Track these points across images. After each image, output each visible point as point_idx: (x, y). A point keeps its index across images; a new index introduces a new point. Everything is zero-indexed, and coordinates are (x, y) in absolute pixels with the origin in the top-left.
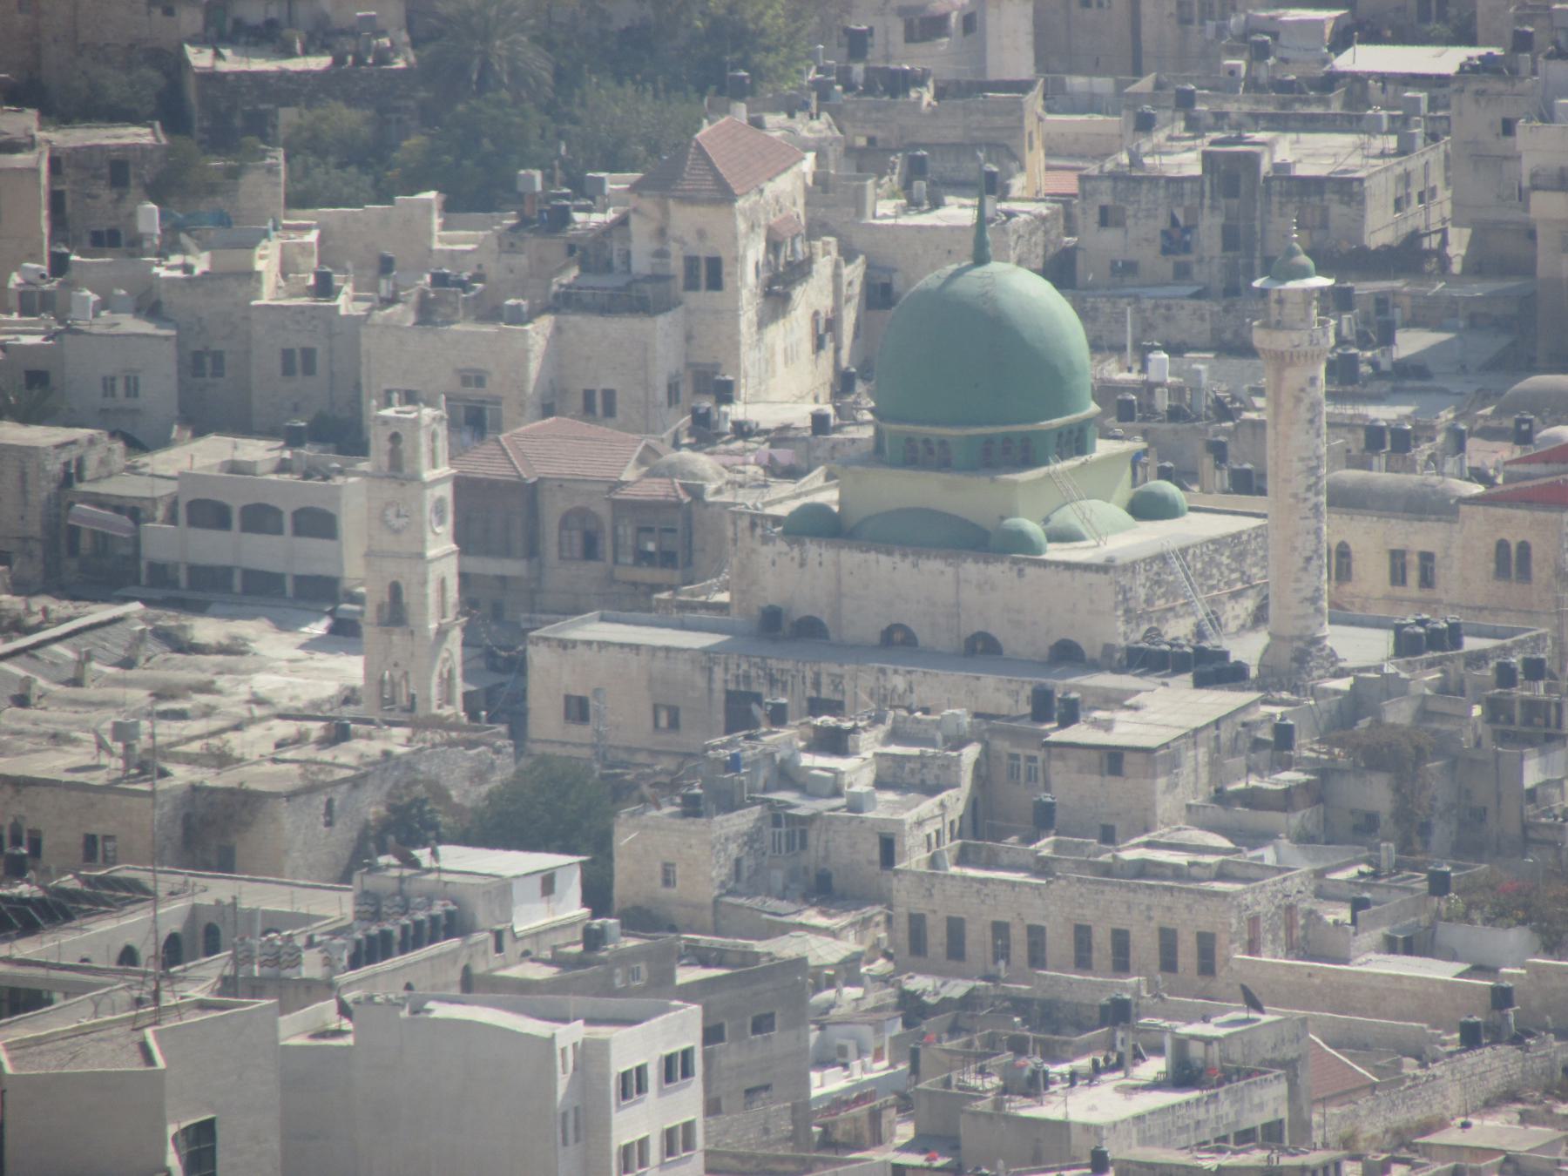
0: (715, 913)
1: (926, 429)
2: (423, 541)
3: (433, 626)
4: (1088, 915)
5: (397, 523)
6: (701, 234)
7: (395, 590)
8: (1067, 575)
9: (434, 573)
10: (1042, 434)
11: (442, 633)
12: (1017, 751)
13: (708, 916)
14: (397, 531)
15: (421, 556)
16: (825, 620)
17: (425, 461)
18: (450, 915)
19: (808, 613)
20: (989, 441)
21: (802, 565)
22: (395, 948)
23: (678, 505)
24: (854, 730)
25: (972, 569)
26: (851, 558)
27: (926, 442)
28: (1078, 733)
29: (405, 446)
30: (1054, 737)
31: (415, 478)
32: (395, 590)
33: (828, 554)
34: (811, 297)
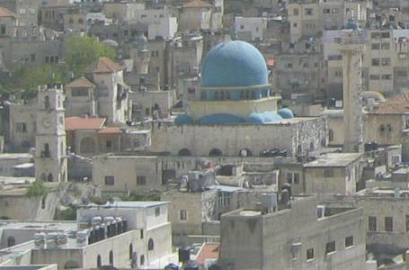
0: (202, 228)
1: (223, 88)
2: (56, 130)
3: (59, 157)
4: (375, 213)
5: (48, 125)
6: (103, 82)
7: (47, 146)
8: (275, 128)
9: (59, 140)
10: (257, 89)
11: (62, 159)
12: (290, 172)
13: (200, 229)
14: (47, 128)
15: (56, 134)
16: (190, 149)
17: (57, 105)
18: (125, 222)
19: (183, 147)
20: (242, 91)
21: (182, 132)
22: (106, 236)
23: (119, 133)
24: (234, 166)
25: (241, 129)
26: (198, 128)
27: (222, 92)
28: (314, 163)
29: (51, 100)
30: (305, 165)
31: (53, 109)
32: (47, 146)
33: (191, 128)
34: (124, 104)
